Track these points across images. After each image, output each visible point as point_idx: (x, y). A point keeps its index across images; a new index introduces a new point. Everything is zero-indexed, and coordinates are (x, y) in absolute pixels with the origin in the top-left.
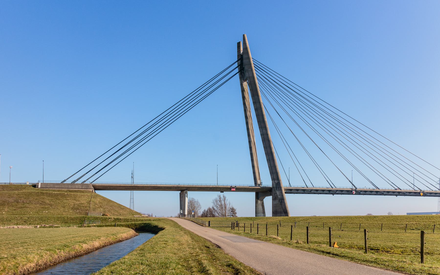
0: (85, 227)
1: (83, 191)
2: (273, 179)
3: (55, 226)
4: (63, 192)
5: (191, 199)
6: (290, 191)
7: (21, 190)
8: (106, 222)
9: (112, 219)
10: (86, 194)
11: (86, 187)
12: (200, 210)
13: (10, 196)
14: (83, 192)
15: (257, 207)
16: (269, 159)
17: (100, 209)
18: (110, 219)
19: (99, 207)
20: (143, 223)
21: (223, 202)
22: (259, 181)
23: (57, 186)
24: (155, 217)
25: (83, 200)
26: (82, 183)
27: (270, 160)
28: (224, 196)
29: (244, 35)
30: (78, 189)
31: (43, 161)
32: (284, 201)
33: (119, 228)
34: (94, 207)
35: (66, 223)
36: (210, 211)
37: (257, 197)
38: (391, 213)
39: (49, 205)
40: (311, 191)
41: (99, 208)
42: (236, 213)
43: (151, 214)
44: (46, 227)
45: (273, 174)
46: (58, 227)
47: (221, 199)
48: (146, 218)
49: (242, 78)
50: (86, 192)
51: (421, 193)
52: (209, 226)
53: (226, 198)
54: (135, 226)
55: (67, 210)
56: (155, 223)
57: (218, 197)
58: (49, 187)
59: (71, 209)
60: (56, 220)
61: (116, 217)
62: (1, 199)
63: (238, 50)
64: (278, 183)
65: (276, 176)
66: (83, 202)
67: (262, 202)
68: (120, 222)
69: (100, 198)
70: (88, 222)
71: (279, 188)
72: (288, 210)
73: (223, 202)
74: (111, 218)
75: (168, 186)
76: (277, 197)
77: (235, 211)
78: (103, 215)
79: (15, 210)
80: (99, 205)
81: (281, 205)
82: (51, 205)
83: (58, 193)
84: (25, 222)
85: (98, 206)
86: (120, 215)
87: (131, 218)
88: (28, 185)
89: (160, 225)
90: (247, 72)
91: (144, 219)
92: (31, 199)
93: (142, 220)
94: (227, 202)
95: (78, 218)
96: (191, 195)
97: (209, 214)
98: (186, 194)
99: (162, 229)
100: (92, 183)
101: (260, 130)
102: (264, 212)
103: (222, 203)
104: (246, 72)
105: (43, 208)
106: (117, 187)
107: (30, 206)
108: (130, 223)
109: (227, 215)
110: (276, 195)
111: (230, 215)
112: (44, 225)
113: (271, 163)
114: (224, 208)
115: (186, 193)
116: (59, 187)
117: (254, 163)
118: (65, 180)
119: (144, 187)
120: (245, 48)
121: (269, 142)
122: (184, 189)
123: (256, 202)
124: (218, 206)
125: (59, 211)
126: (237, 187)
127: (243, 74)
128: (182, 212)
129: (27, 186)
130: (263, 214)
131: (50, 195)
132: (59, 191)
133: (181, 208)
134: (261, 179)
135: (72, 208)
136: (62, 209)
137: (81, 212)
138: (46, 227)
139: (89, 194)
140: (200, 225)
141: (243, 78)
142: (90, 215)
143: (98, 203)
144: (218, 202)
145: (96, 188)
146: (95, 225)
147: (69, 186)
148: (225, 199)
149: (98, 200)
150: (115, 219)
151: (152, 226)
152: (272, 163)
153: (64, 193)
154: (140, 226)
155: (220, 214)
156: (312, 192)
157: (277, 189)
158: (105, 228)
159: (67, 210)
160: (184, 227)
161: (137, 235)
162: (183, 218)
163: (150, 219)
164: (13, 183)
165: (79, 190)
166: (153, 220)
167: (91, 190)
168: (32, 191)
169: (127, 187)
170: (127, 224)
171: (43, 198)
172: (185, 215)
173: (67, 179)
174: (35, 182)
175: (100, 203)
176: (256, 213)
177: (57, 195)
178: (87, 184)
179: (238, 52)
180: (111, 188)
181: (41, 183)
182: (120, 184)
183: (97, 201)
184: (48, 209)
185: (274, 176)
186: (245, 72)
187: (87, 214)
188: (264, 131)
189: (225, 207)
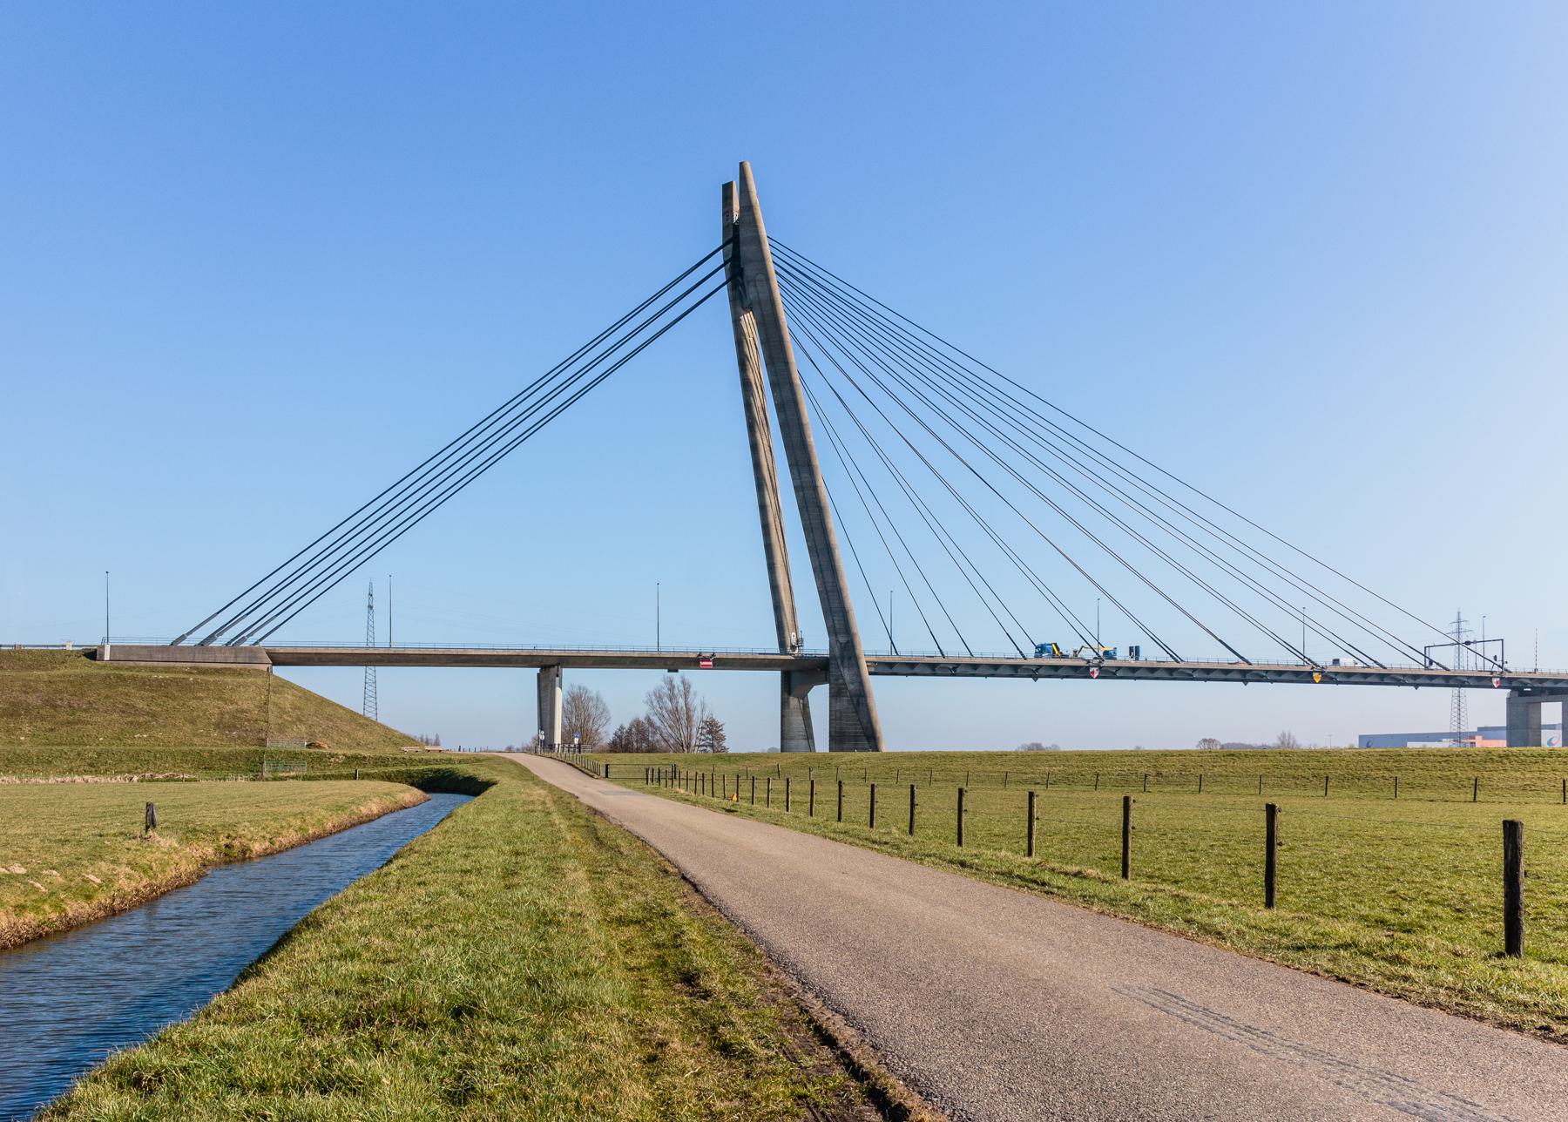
0: (267, 780)
2: (832, 631)
5: (576, 690)
6: (887, 668)
7: (53, 668)
12: (607, 726)
13: (27, 688)
14: (239, 673)
15: (785, 719)
16: (820, 565)
20: (431, 770)
21: (681, 702)
22: (794, 633)
23: (159, 656)
24: (459, 750)
25: (247, 700)
27: (822, 572)
28: (683, 682)
29: (742, 165)
30: (223, 665)
32: (866, 701)
33: (366, 782)
34: (280, 722)
35: (210, 769)
36: (638, 731)
37: (787, 688)
38: (1289, 738)
39: (148, 714)
40: (954, 669)
42: (722, 738)
44: (158, 780)
45: (833, 616)
47: (676, 691)
49: (738, 302)
50: (250, 673)
51: (1315, 675)
52: (607, 776)
53: (689, 687)
54: (410, 777)
56: (468, 770)
57: (665, 683)
61: (349, 753)
62: (4, 697)
63: (726, 210)
64: (848, 642)
65: (843, 622)
66: (245, 707)
67: (801, 701)
68: (364, 767)
71: (849, 658)
72: (878, 729)
73: (681, 702)
75: (501, 653)
76: (843, 689)
77: (722, 732)
78: (309, 746)
79: (52, 730)
81: (857, 712)
82: (154, 716)
84: (91, 765)
85: (290, 719)
87: (393, 754)
88: (72, 651)
89: (483, 774)
90: (752, 284)
91: (432, 758)
93: (427, 762)
94: (695, 702)
95: (240, 753)
96: (571, 678)
97: (637, 742)
98: (557, 679)
99: (488, 785)
101: (792, 473)
102: (809, 736)
103: (679, 704)
104: (748, 282)
105: (132, 723)
108: (394, 769)
109: (695, 746)
110: (841, 681)
111: (702, 743)
114: (684, 722)
115: (557, 676)
117: (775, 577)
120: (747, 207)
122: (549, 663)
123: (784, 704)
124: (666, 715)
126: (717, 656)
127: (740, 288)
128: (542, 737)
130: (804, 743)
131: (144, 684)
132: (167, 670)
133: (541, 727)
134: (800, 628)
136: (188, 728)
138: (158, 780)
139: (260, 681)
140: (587, 774)
141: (740, 301)
144: (666, 699)
145: (278, 659)
146: (292, 774)
147: (197, 655)
148: (688, 692)
150: (349, 758)
151: (460, 778)
152: (829, 579)
153: (185, 676)
155: (672, 741)
156: (958, 670)
157: (846, 664)
158: (322, 783)
160: (545, 779)
162: (546, 754)
164: (24, 646)
165: (228, 666)
166: (460, 762)
167: (264, 667)
168: (87, 670)
169: (374, 656)
172: (552, 747)
173: (188, 634)
174: (93, 641)
176: (784, 737)
178: (249, 650)
181: (111, 646)
183: (287, 703)
184: (147, 727)
185: (836, 622)
186: (746, 285)
187: (262, 742)
188: (805, 475)
189: (689, 718)
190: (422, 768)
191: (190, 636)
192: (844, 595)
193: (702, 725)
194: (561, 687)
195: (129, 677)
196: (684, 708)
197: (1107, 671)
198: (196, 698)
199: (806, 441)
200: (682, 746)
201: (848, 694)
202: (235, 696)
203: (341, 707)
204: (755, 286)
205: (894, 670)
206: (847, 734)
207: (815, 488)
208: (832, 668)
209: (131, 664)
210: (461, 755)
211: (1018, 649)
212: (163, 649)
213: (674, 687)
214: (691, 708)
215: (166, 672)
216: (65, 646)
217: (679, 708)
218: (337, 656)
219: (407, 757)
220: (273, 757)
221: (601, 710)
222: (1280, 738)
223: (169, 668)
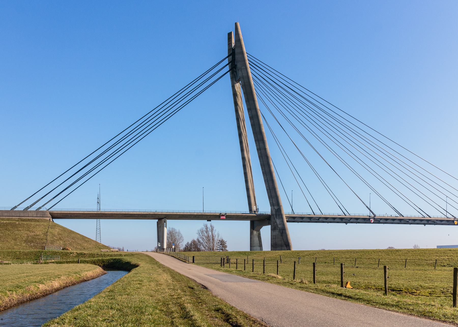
0: (42, 263)
2: (272, 205)
3: (5, 262)
6: (293, 219)
8: (67, 258)
9: (75, 254)
10: (42, 223)
11: (42, 215)
14: (38, 221)
17: (60, 242)
20: (112, 259)
21: (210, 233)
22: (255, 207)
25: (39, 231)
27: (268, 181)
28: (211, 226)
29: (236, 24)
30: (32, 218)
34: (52, 239)
35: (19, 259)
37: (253, 227)
40: (319, 219)
42: (226, 247)
46: (8, 264)
47: (208, 230)
48: (116, 253)
49: (234, 79)
50: (42, 221)
51: (455, 221)
52: (193, 262)
53: (213, 228)
54: (103, 262)
55: (18, 243)
56: (128, 259)
57: (204, 226)
61: (79, 252)
63: (229, 43)
64: (278, 209)
65: (276, 201)
66: (38, 233)
67: (258, 232)
68: (85, 258)
70: (45, 257)
71: (279, 215)
72: (290, 242)
73: (210, 233)
74: (73, 253)
76: (276, 227)
77: (226, 244)
78: (63, 249)
80: (58, 237)
85: (56, 239)
86: (84, 249)
89: (133, 261)
91: (113, 254)
93: (111, 256)
94: (215, 233)
95: (32, 252)
96: (170, 224)
97: (194, 248)
98: (165, 223)
99: (136, 266)
100: (49, 210)
101: (256, 143)
102: (261, 246)
108: (97, 259)
109: (216, 249)
111: (218, 248)
113: (269, 185)
114: (211, 240)
115: (165, 222)
116: (8, 215)
118: (16, 206)
120: (238, 40)
121: (267, 158)
123: (251, 233)
124: (205, 238)
125: (10, 244)
126: (227, 214)
127: (235, 73)
128: (159, 245)
130: (259, 248)
132: (8, 220)
133: (159, 241)
136: (13, 242)
137: (37, 245)
139: (45, 224)
140: (182, 261)
141: (235, 78)
144: (205, 232)
145: (55, 216)
146: (53, 261)
147: (21, 214)
148: (213, 230)
150: (78, 254)
151: (124, 262)
153: (15, 222)
154: (109, 262)
155: (207, 248)
156: (320, 220)
159: (18, 243)
165: (34, 218)
166: (125, 256)
167: (48, 219)
170: (93, 260)
175: (59, 234)
176: (252, 246)
177: (7, 224)
178: (43, 212)
179: (229, 46)
180: (72, 216)
185: (273, 201)
187: (43, 248)
188: (261, 144)
189: (213, 239)
190: (109, 258)
192: (277, 190)
193: (218, 241)
194: (166, 227)
196: (211, 235)
197: (376, 220)
199: (261, 131)
200: (211, 250)
201: (278, 229)
203: (79, 234)
204: (241, 71)
205: (295, 220)
206: (278, 244)
207: (265, 149)
208: (272, 218)
210: (128, 253)
211: (343, 212)
213: (208, 228)
214: (214, 236)
215: (8, 220)
217: (210, 236)
218: (78, 214)
220: (46, 254)
221: (180, 237)
222: (414, 247)
223: (9, 219)
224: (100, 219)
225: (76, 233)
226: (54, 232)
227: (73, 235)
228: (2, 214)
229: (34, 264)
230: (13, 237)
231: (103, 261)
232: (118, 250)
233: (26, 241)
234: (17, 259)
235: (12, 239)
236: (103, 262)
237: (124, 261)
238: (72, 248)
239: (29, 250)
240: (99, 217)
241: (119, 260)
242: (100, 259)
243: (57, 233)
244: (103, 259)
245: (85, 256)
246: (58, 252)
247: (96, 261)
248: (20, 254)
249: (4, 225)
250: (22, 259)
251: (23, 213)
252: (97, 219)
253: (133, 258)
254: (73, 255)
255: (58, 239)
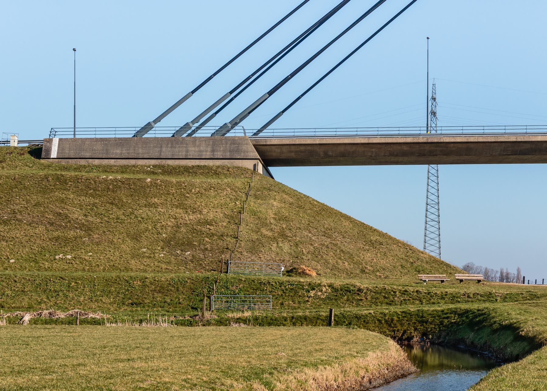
0: (208, 323)
1: (218, 167)
3: (91, 315)
4: (138, 172)
8: (296, 305)
9: (324, 289)
10: (226, 180)
11: (230, 151)
14: (215, 172)
17: (280, 245)
18: (314, 289)
19: (274, 238)
20: (454, 312)
26: (213, 135)
31: (74, 50)
34: (255, 237)
35: (138, 304)
41: (275, 239)
43: (513, 272)
46: (95, 322)
48: (473, 289)
50: (229, 172)
54: (422, 322)
55: (144, 250)
58: (88, 155)
59: (162, 243)
60: (98, 290)
61: (338, 283)
66: (211, 216)
68: (358, 305)
69: (285, 196)
70: (224, 300)
74: (319, 285)
78: (289, 272)
80: (277, 229)
82: (88, 229)
83: (119, 177)
85: (270, 234)
86: (363, 271)
87: (404, 286)
88: (15, 148)
91: (462, 292)
92: (18, 204)
93: (454, 298)
95: (182, 282)
100: (261, 134)
105: (57, 239)
106: (354, 148)
107: (13, 234)
108: (398, 309)
112: (50, 314)
116: (125, 153)
118: (149, 124)
119: (472, 146)
125: (117, 253)
129: (11, 151)
132: (124, 169)
135: (167, 242)
136: (127, 246)
137: (202, 256)
139: (239, 183)
142: (236, 269)
143: (272, 221)
146: (247, 314)
149: (273, 206)
150: (336, 290)
154: (442, 323)
159: (144, 250)
161: (403, 376)
163: (490, 294)
166: (505, 299)
167: (249, 164)
168: (27, 171)
170: (385, 315)
171: (62, 201)
175: (280, 218)
177: (116, 185)
178: (233, 141)
180: (330, 153)
181: (60, 140)
182: (369, 136)
183: (270, 211)
191: (158, 124)
195: (71, 179)
198: (149, 205)
202: (200, 202)
209: (83, 162)
212: (121, 142)
215: (123, 172)
216: (8, 142)
218: (348, 148)
219: (423, 290)
224: (439, 165)
225: (341, 213)
226: (264, 211)
227: (328, 222)
228: (107, 150)
229: (183, 324)
230: (131, 229)
231: (422, 317)
232: (482, 278)
233: (169, 242)
234: (132, 304)
235: (128, 236)
236: (419, 322)
237: (495, 322)
238: (319, 267)
239: (173, 275)
240: (424, 155)
241: (482, 317)
242: (412, 310)
243: (275, 214)
244: (423, 311)
245: (361, 300)
246: (269, 283)
247: (395, 318)
248: (145, 286)
249: (108, 188)
250: (149, 306)
251: (171, 147)
252: (429, 163)
253: (535, 309)
254: (319, 293)
255: (276, 235)
